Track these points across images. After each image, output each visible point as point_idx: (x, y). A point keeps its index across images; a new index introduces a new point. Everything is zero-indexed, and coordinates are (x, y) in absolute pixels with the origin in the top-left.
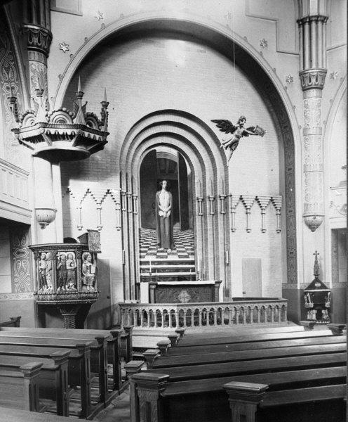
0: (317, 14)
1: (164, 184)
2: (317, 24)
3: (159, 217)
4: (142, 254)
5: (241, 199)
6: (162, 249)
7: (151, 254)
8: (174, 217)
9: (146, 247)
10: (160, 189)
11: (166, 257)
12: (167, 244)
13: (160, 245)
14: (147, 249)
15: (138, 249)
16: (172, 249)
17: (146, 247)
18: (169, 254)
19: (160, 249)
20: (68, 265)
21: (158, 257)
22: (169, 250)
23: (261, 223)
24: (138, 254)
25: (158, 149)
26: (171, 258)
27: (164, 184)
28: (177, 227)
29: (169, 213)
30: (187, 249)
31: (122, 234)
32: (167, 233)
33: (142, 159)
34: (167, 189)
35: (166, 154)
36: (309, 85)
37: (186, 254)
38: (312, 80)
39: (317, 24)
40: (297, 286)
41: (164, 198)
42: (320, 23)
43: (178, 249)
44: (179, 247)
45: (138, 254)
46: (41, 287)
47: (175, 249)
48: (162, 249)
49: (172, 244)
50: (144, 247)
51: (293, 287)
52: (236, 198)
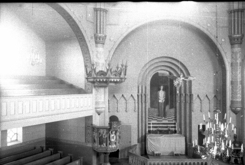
0: (238, 8)
1: (162, 87)
2: (238, 13)
3: (159, 103)
4: (150, 120)
5: (198, 96)
6: (160, 117)
7: (155, 120)
8: (166, 102)
9: (152, 117)
10: (159, 90)
11: (162, 121)
12: (162, 115)
13: (159, 116)
14: (152, 117)
15: (147, 116)
16: (165, 117)
17: (152, 117)
18: (163, 120)
19: (159, 117)
20: (103, 136)
21: (169, 121)
22: (163, 118)
23: (209, 107)
24: (147, 120)
25: (159, 72)
26: (164, 122)
27: (162, 87)
28: (167, 107)
29: (164, 101)
30: (172, 118)
31: (138, 115)
32: (163, 110)
33: (154, 73)
34: (163, 90)
35: (163, 74)
36: (234, 42)
37: (172, 120)
38: (235, 40)
39: (238, 13)
40: (200, 147)
41: (162, 94)
42: (240, 13)
43: (167, 117)
44: (168, 117)
45: (147, 120)
46: (94, 143)
47: (166, 117)
48: (160, 117)
49: (165, 115)
50: (151, 117)
51: (200, 147)
52: (195, 96)
